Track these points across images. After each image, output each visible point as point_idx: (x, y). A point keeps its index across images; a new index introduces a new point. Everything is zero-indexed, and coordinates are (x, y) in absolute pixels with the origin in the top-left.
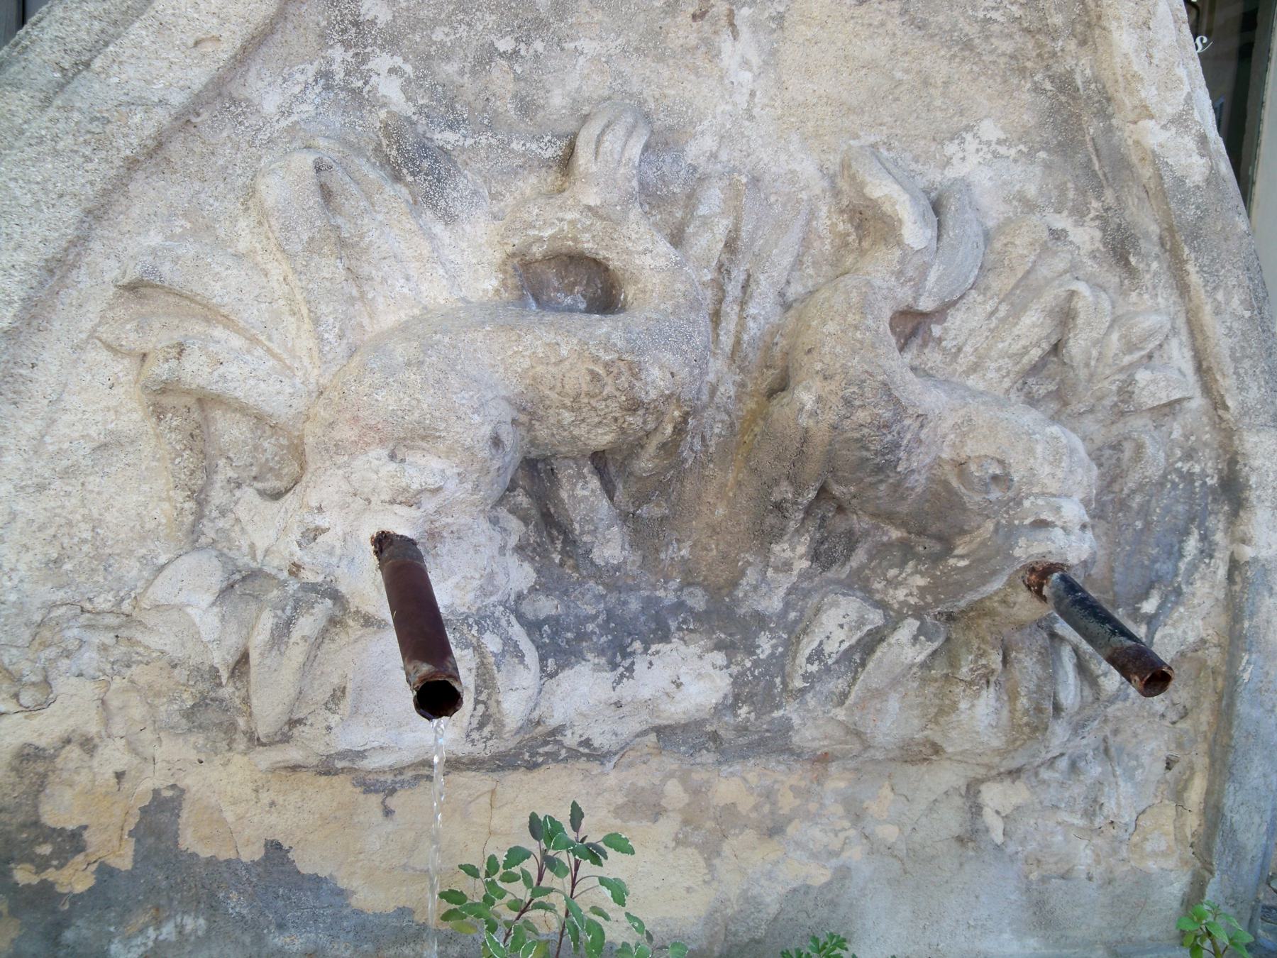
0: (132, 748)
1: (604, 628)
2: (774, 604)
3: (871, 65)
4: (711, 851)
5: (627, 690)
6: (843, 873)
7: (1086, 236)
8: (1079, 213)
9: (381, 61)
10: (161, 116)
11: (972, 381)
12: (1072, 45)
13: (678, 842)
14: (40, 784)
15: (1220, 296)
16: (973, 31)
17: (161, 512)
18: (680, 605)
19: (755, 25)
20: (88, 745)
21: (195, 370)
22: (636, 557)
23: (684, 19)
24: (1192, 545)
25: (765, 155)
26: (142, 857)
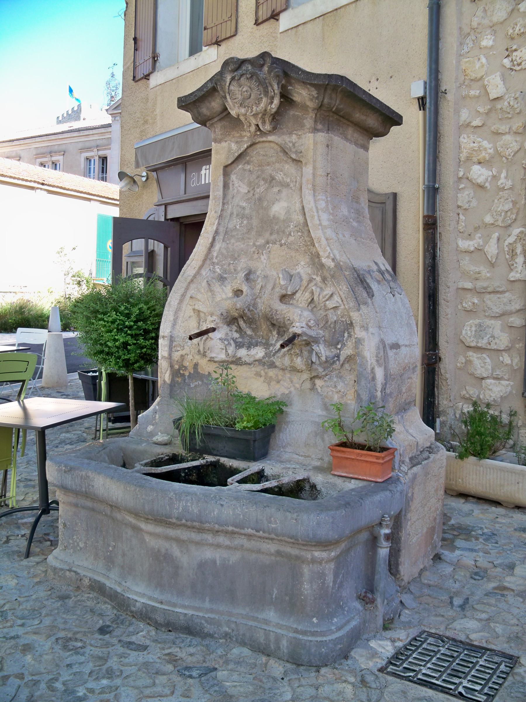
0: (193, 356)
1: (248, 344)
2: (274, 342)
3: (283, 256)
4: (269, 384)
5: (249, 353)
6: (290, 392)
7: (318, 279)
8: (317, 275)
9: (217, 267)
10: (191, 277)
11: (300, 305)
12: (312, 247)
13: (264, 382)
14: (183, 360)
15: (340, 287)
16: (298, 247)
17: (195, 325)
18: (261, 342)
19: (266, 253)
20: (188, 355)
21: (196, 307)
22: (254, 334)
23: (256, 254)
24: (346, 335)
25: (268, 272)
26: (194, 372)
